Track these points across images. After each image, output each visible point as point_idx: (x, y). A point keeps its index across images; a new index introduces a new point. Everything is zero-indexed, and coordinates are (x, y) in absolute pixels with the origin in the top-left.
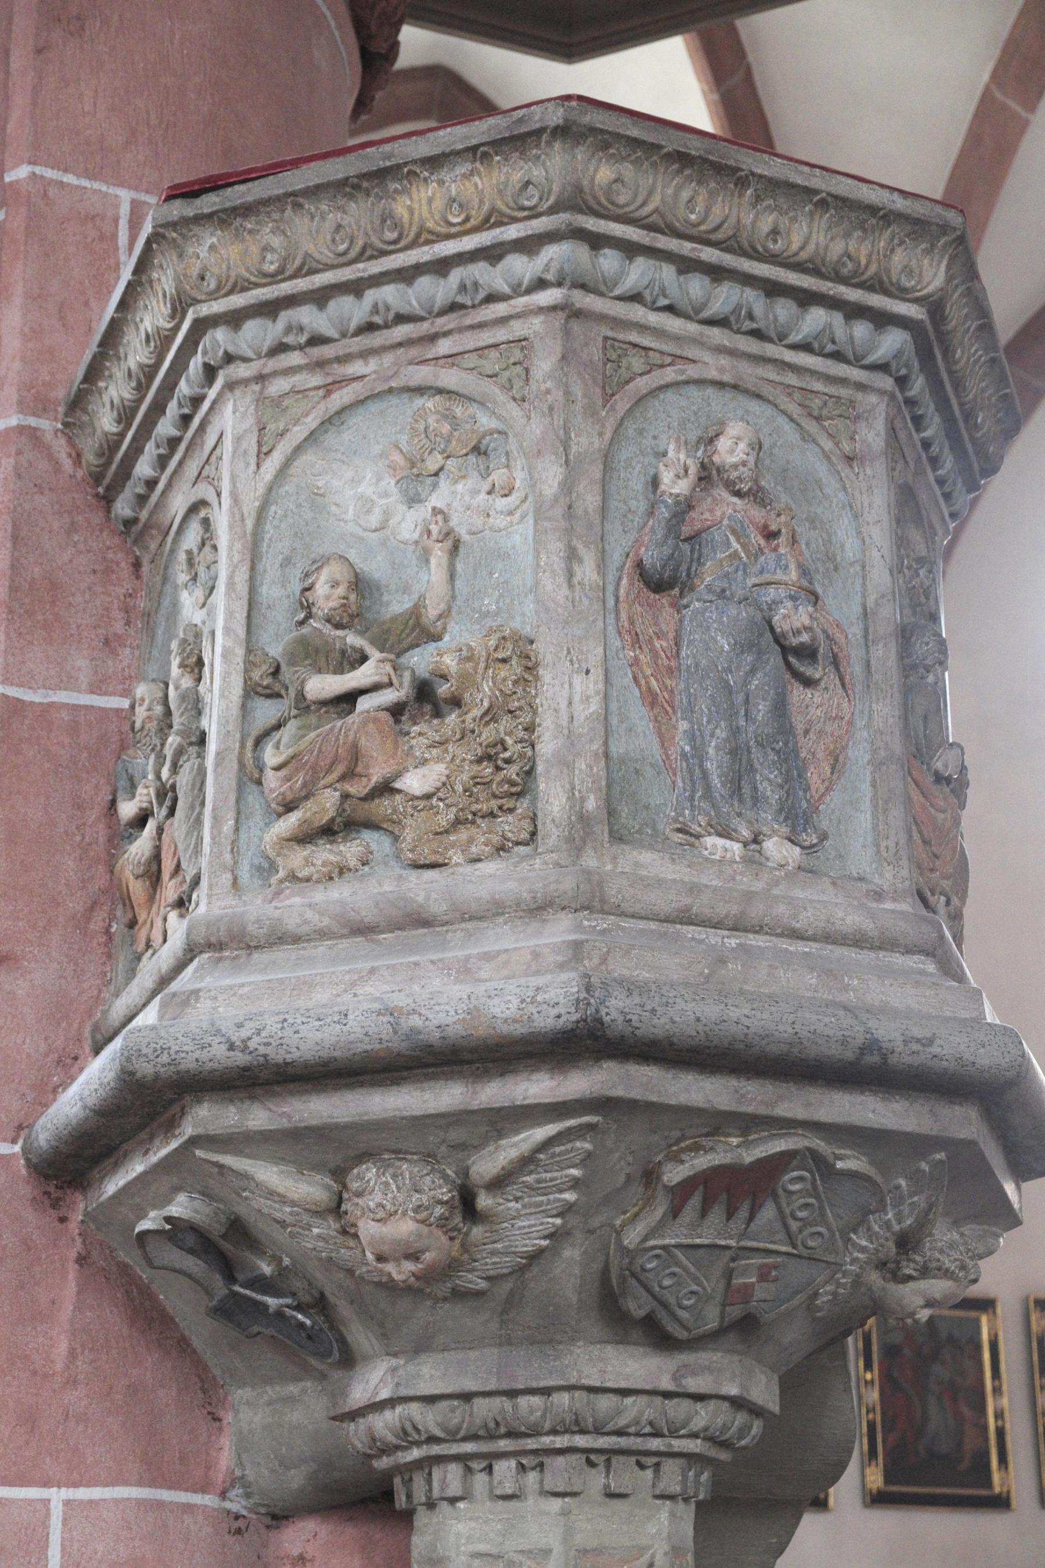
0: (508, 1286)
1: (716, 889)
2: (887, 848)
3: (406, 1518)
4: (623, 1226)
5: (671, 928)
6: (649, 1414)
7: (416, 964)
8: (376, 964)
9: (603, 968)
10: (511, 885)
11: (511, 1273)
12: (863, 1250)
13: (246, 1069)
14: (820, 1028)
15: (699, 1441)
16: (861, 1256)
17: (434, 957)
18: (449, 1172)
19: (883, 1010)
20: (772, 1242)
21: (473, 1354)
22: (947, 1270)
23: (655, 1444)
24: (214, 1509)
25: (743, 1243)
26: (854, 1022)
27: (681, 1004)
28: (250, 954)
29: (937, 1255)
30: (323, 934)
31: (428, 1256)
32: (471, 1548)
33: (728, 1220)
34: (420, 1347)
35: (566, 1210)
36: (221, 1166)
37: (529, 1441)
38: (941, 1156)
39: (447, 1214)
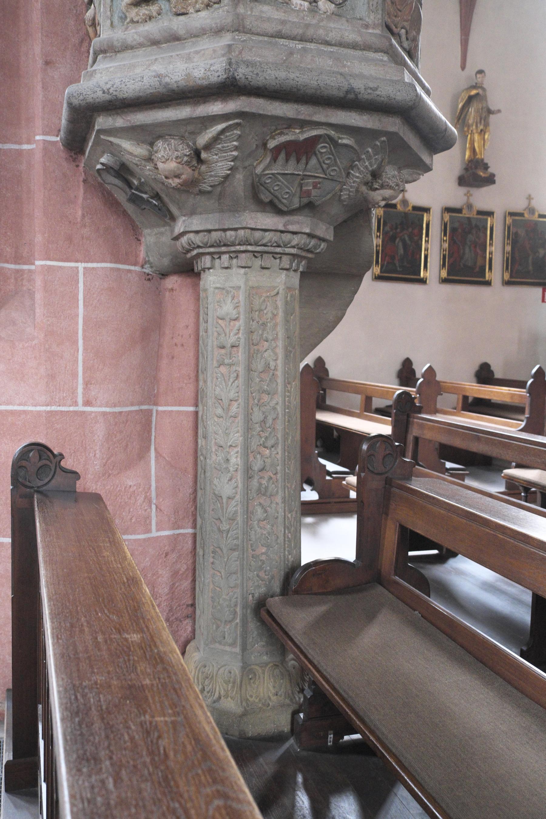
0: (219, 189)
1: (294, 22)
2: (373, 5)
3: (198, 275)
4: (257, 165)
5: (273, 40)
6: (275, 238)
7: (171, 56)
8: (157, 57)
9: (240, 56)
10: (208, 21)
11: (218, 184)
12: (358, 177)
13: (110, 101)
14: (328, 82)
15: (296, 249)
16: (357, 180)
17: (178, 53)
18: (190, 143)
19: (361, 76)
20: (317, 173)
21: (210, 215)
22: (391, 186)
23: (278, 250)
24: (139, 272)
25: (305, 173)
26: (343, 80)
27: (269, 71)
28: (116, 55)
29: (387, 180)
30: (141, 45)
31: (183, 177)
32: (214, 286)
33: (298, 163)
34: (192, 213)
35: (235, 159)
36: (111, 142)
37: (232, 248)
38: (384, 139)
39: (189, 160)
